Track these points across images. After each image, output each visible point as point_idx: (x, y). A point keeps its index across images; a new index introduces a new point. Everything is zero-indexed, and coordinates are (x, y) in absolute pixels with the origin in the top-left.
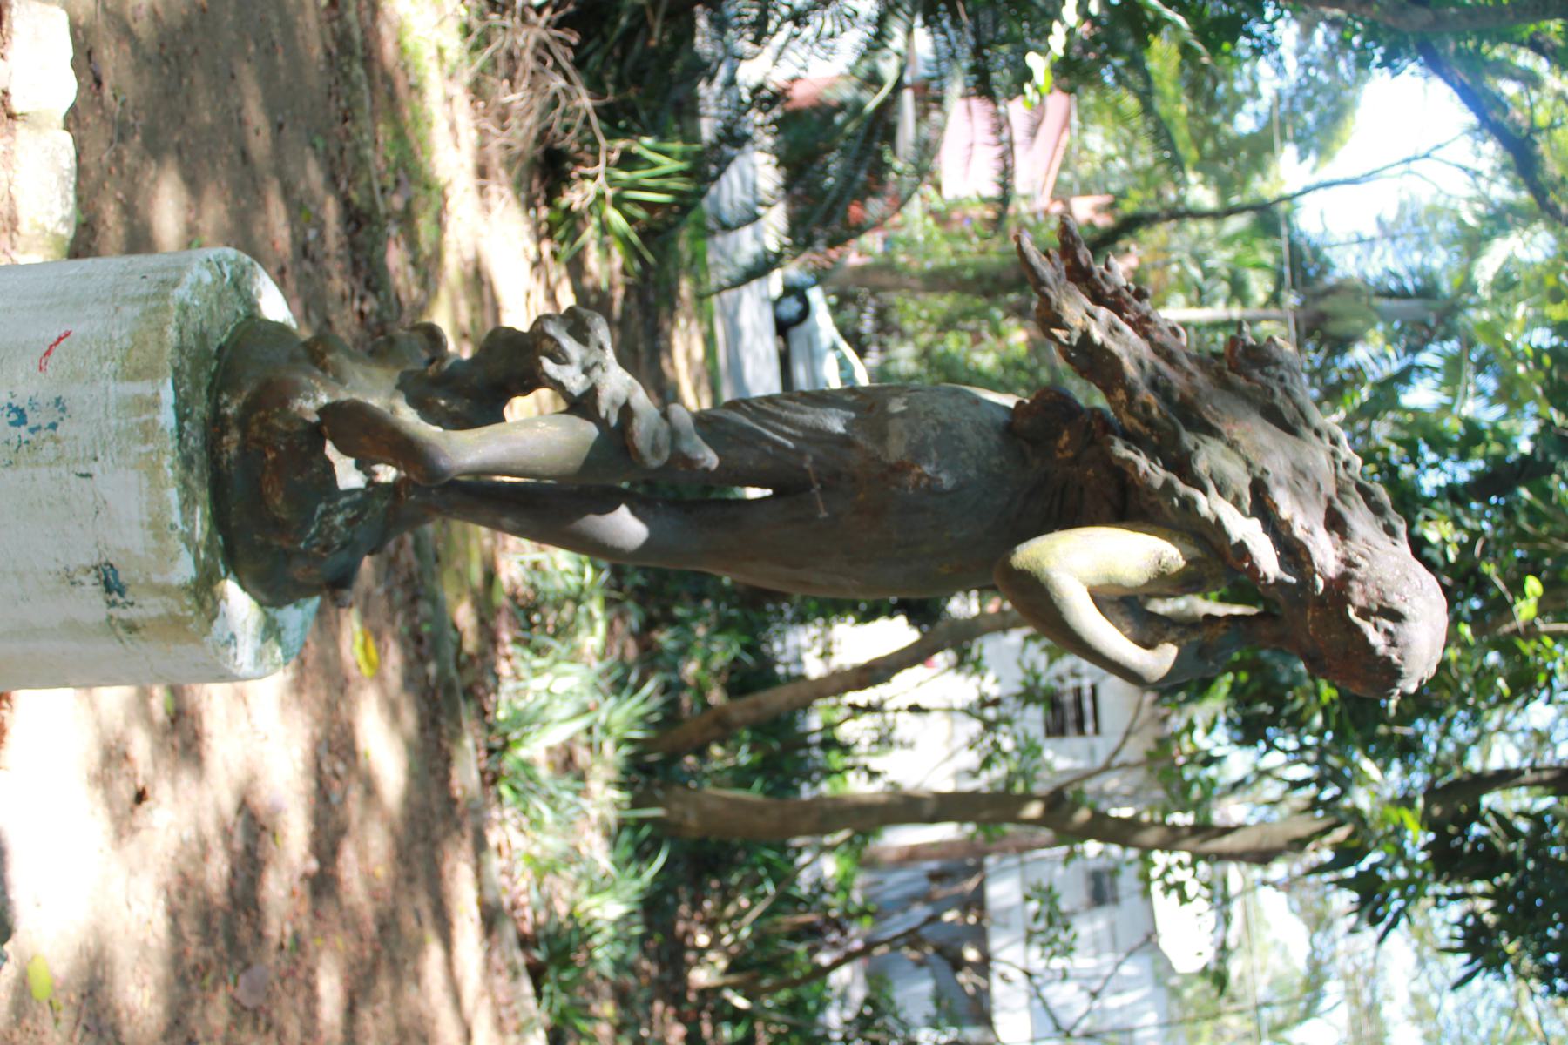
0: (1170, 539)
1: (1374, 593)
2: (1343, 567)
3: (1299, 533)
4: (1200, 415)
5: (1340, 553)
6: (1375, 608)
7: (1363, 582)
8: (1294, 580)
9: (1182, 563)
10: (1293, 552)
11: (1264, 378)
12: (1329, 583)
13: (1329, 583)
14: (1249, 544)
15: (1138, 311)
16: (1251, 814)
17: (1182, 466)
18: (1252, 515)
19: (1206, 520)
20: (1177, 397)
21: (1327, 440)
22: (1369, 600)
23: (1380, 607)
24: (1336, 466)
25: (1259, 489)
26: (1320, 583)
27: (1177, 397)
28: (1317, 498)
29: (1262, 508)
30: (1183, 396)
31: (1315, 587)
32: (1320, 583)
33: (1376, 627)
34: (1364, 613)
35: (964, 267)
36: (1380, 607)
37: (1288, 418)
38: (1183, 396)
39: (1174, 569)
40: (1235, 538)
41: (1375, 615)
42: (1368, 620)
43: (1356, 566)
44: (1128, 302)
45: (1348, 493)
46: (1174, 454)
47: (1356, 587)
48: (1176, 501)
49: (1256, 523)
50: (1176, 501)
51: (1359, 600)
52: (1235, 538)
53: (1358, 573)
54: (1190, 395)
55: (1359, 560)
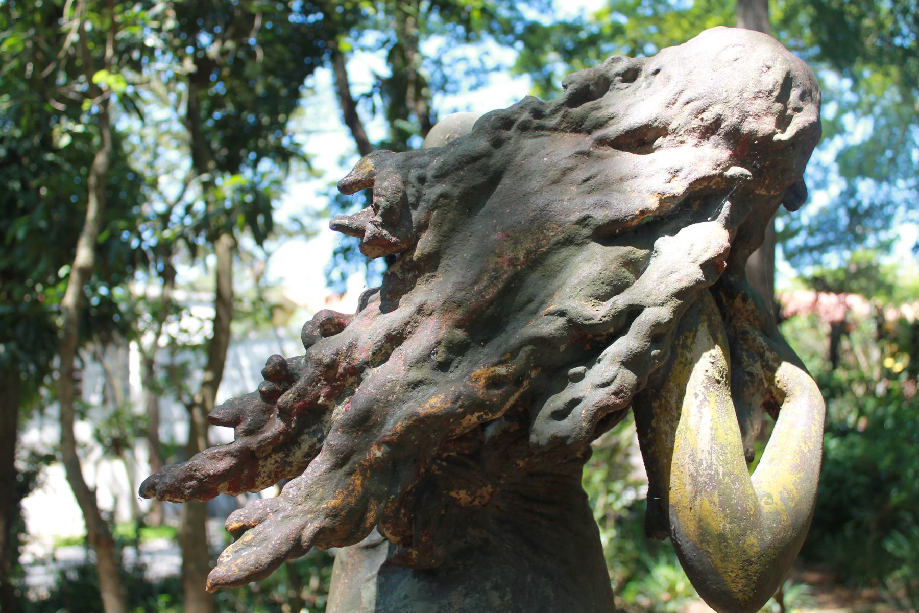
0: (688, 366)
1: (760, 105)
2: (714, 138)
3: (678, 187)
4: (490, 303)
5: (691, 140)
6: (778, 106)
7: (744, 117)
8: (727, 204)
9: (717, 351)
10: (694, 204)
11: (423, 204)
12: (737, 159)
13: (737, 159)
14: (702, 259)
15: (313, 381)
16: (368, 277)
17: (587, 342)
18: (650, 246)
19: (676, 311)
20: (460, 334)
21: (506, 134)
22: (768, 111)
23: (778, 99)
24: (541, 128)
25: (613, 233)
26: (736, 171)
27: (460, 334)
28: (600, 158)
29: (643, 230)
30: (459, 325)
31: (742, 177)
32: (736, 171)
33: (798, 110)
34: (783, 121)
35: (23, 574)
36: (778, 99)
37: (480, 180)
38: (459, 325)
39: (723, 362)
40: (698, 275)
41: (786, 109)
42: (791, 118)
43: (718, 121)
44: (301, 395)
45: (583, 119)
46: (562, 348)
47: (748, 126)
48: (654, 352)
49: (663, 243)
50: (654, 352)
51: (766, 125)
52: (698, 275)
53: (731, 120)
54: (458, 314)
55: (709, 116)
